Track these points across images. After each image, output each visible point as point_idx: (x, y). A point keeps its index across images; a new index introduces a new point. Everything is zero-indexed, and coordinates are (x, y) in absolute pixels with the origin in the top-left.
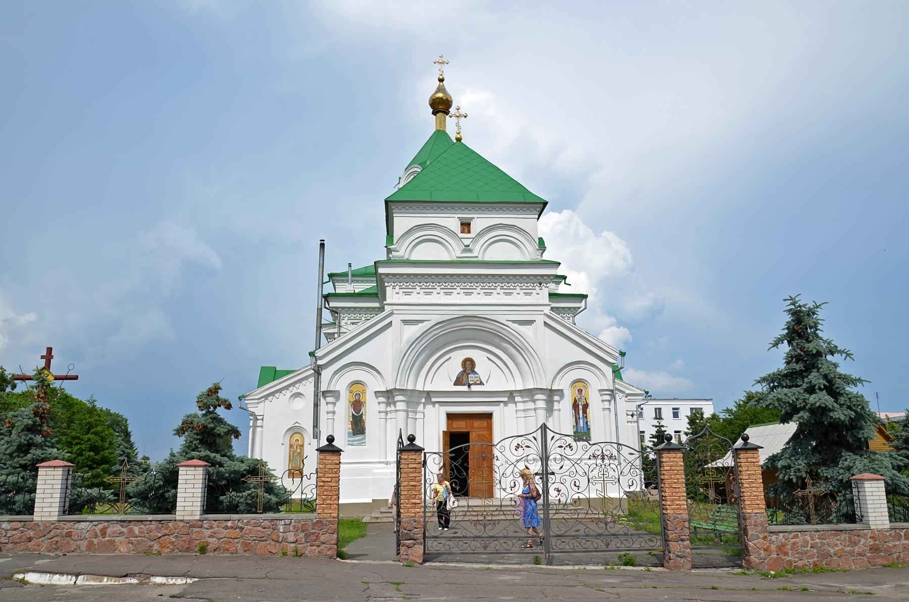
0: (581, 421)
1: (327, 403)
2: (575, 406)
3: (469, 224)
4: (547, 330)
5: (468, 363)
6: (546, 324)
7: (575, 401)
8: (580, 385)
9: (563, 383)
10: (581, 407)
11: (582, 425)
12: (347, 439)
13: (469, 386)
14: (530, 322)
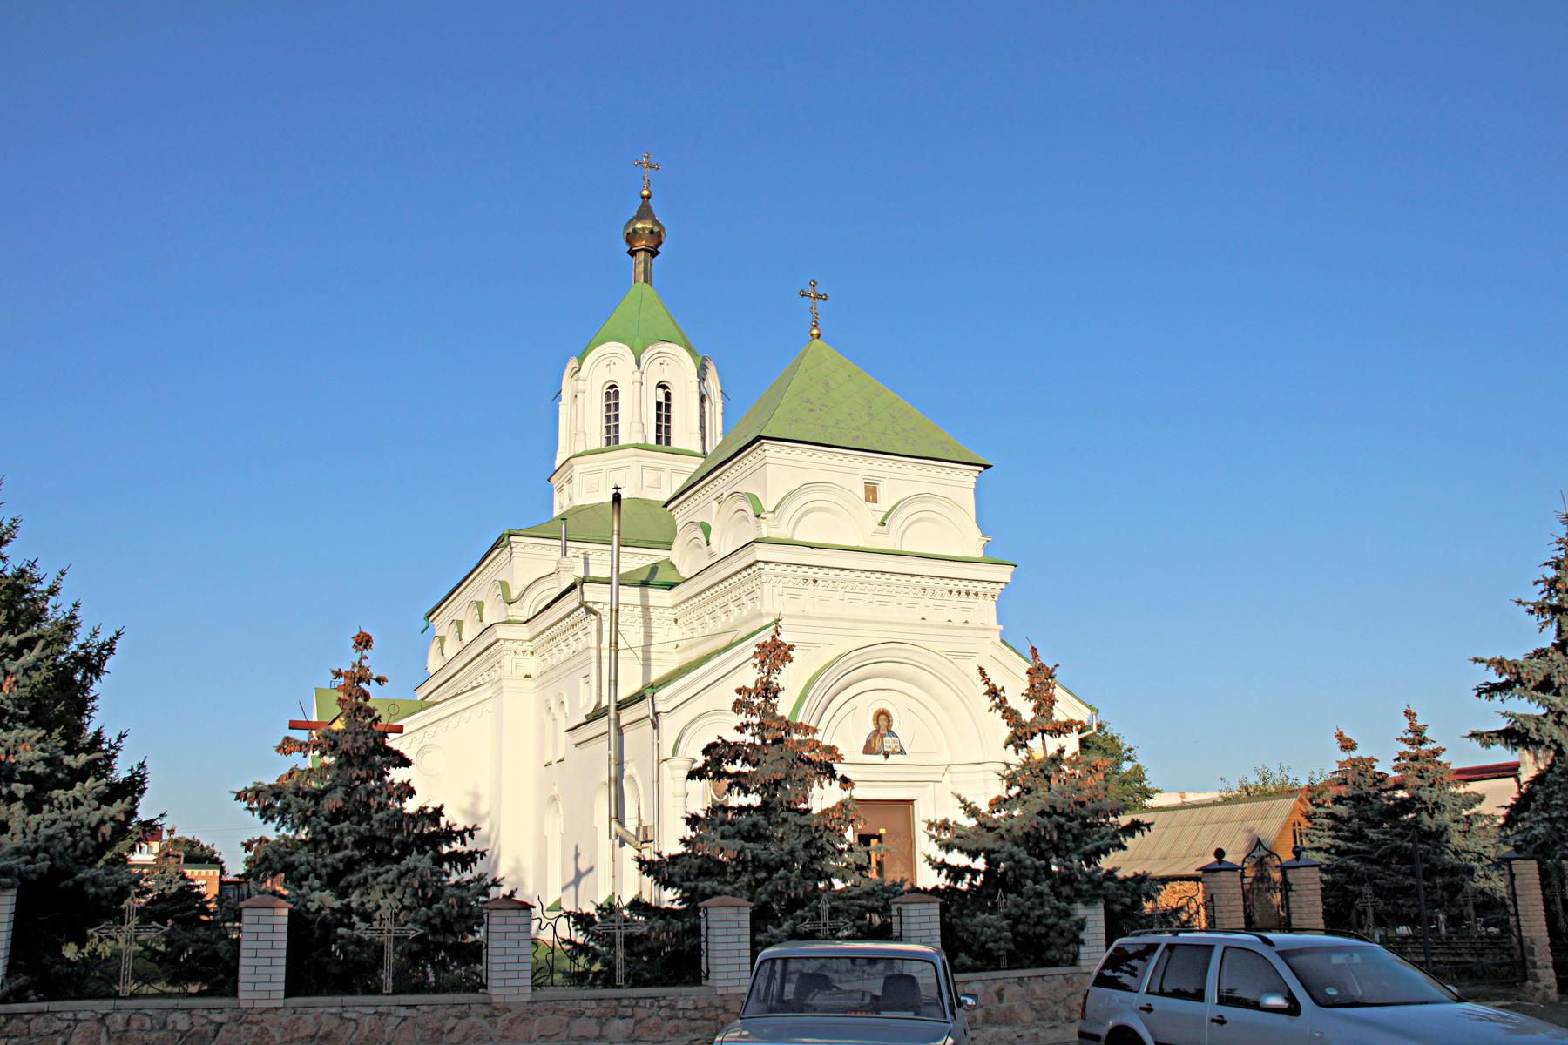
13: (887, 755)
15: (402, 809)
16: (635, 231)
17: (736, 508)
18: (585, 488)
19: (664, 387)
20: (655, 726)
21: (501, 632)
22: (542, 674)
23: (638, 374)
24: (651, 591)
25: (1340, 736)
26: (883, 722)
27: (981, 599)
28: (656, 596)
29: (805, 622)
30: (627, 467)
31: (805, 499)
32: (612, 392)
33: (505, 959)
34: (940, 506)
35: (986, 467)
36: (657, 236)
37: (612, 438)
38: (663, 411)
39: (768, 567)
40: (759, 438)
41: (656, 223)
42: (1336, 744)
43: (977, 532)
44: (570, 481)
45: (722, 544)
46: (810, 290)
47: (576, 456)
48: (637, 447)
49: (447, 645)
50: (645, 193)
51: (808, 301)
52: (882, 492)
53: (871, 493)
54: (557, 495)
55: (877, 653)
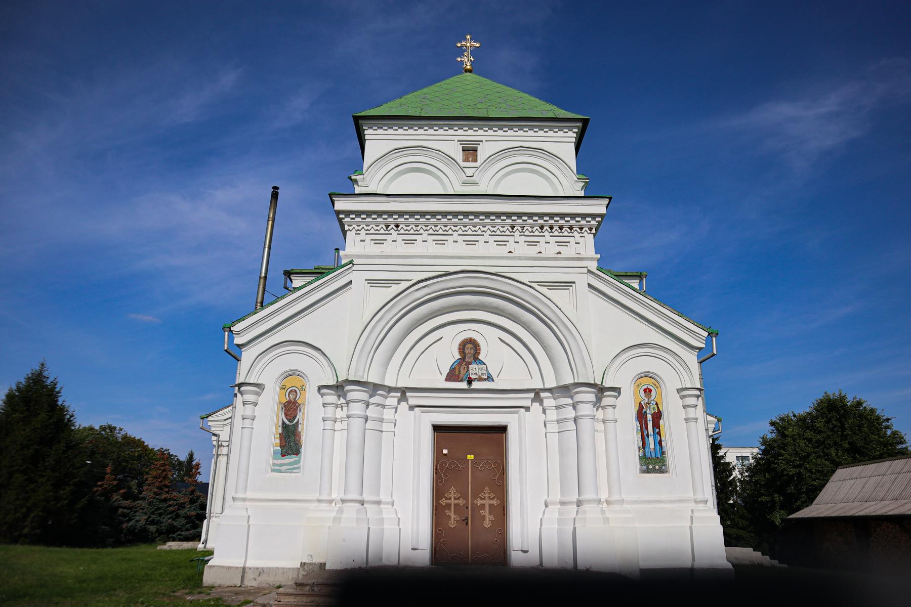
0: (651, 439)
1: (244, 403)
2: (641, 415)
3: (475, 150)
4: (593, 297)
6: (589, 285)
7: (641, 407)
8: (648, 385)
9: (623, 377)
10: (649, 417)
11: (652, 446)
12: (271, 461)
13: (470, 382)
14: (568, 284)
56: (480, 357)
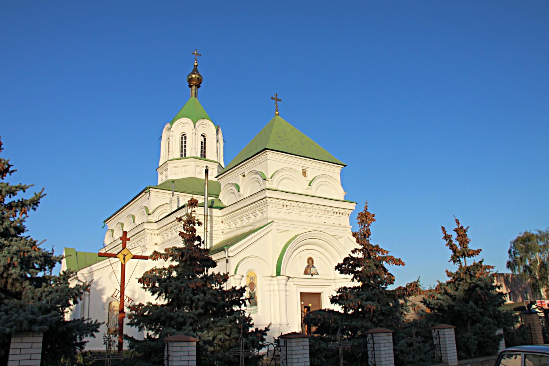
5: (310, 260)
13: (312, 275)
15: (221, 288)
16: (192, 78)
17: (252, 177)
18: (176, 171)
19: (204, 136)
20: (227, 262)
21: (146, 226)
22: (163, 243)
23: (194, 130)
24: (214, 210)
25: (447, 272)
26: (310, 262)
27: (344, 215)
28: (215, 212)
29: (283, 222)
30: (190, 165)
31: (285, 173)
32: (184, 137)
33: (20, 357)
34: (328, 179)
35: (345, 166)
36: (200, 81)
37: (183, 155)
38: (203, 145)
39: (270, 200)
40: (266, 149)
41: (200, 75)
42: (446, 274)
43: (342, 190)
44: (166, 170)
45: (245, 192)
46: (274, 97)
47: (169, 160)
48: (194, 158)
49: (115, 233)
50: (196, 64)
51: (274, 101)
52: (308, 173)
53: (304, 173)
54: (160, 176)
55: (317, 235)
56: (314, 265)
